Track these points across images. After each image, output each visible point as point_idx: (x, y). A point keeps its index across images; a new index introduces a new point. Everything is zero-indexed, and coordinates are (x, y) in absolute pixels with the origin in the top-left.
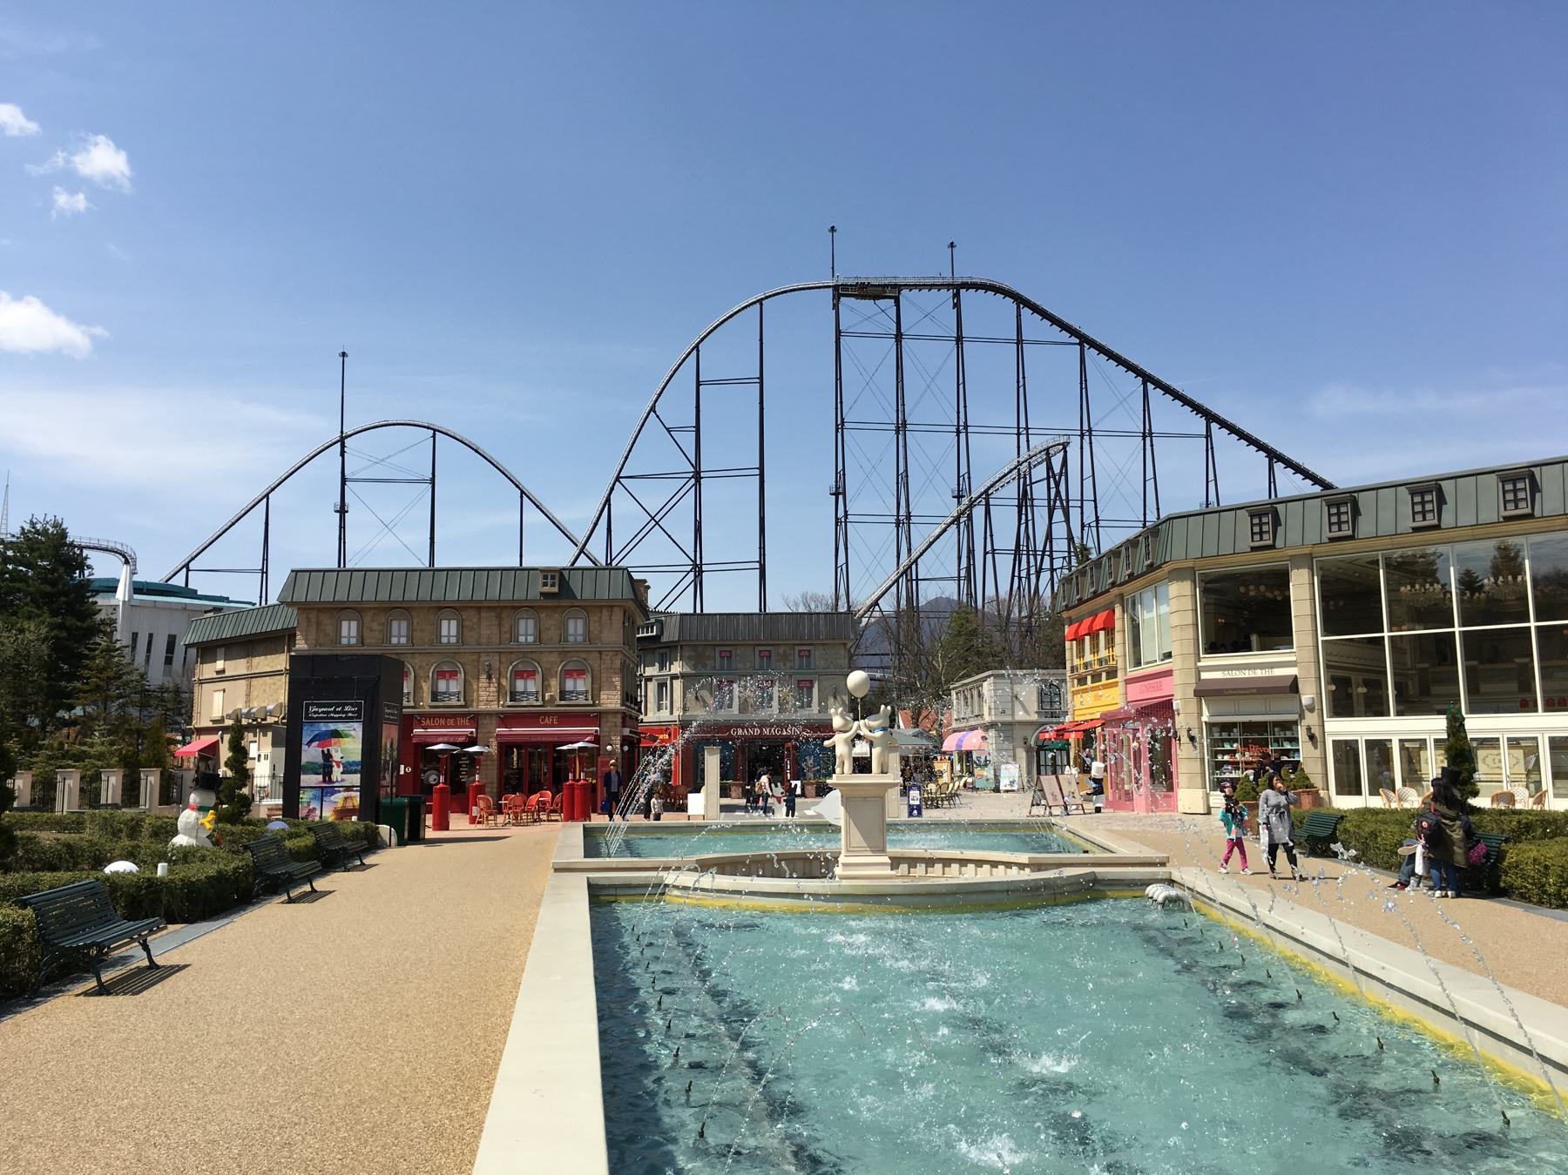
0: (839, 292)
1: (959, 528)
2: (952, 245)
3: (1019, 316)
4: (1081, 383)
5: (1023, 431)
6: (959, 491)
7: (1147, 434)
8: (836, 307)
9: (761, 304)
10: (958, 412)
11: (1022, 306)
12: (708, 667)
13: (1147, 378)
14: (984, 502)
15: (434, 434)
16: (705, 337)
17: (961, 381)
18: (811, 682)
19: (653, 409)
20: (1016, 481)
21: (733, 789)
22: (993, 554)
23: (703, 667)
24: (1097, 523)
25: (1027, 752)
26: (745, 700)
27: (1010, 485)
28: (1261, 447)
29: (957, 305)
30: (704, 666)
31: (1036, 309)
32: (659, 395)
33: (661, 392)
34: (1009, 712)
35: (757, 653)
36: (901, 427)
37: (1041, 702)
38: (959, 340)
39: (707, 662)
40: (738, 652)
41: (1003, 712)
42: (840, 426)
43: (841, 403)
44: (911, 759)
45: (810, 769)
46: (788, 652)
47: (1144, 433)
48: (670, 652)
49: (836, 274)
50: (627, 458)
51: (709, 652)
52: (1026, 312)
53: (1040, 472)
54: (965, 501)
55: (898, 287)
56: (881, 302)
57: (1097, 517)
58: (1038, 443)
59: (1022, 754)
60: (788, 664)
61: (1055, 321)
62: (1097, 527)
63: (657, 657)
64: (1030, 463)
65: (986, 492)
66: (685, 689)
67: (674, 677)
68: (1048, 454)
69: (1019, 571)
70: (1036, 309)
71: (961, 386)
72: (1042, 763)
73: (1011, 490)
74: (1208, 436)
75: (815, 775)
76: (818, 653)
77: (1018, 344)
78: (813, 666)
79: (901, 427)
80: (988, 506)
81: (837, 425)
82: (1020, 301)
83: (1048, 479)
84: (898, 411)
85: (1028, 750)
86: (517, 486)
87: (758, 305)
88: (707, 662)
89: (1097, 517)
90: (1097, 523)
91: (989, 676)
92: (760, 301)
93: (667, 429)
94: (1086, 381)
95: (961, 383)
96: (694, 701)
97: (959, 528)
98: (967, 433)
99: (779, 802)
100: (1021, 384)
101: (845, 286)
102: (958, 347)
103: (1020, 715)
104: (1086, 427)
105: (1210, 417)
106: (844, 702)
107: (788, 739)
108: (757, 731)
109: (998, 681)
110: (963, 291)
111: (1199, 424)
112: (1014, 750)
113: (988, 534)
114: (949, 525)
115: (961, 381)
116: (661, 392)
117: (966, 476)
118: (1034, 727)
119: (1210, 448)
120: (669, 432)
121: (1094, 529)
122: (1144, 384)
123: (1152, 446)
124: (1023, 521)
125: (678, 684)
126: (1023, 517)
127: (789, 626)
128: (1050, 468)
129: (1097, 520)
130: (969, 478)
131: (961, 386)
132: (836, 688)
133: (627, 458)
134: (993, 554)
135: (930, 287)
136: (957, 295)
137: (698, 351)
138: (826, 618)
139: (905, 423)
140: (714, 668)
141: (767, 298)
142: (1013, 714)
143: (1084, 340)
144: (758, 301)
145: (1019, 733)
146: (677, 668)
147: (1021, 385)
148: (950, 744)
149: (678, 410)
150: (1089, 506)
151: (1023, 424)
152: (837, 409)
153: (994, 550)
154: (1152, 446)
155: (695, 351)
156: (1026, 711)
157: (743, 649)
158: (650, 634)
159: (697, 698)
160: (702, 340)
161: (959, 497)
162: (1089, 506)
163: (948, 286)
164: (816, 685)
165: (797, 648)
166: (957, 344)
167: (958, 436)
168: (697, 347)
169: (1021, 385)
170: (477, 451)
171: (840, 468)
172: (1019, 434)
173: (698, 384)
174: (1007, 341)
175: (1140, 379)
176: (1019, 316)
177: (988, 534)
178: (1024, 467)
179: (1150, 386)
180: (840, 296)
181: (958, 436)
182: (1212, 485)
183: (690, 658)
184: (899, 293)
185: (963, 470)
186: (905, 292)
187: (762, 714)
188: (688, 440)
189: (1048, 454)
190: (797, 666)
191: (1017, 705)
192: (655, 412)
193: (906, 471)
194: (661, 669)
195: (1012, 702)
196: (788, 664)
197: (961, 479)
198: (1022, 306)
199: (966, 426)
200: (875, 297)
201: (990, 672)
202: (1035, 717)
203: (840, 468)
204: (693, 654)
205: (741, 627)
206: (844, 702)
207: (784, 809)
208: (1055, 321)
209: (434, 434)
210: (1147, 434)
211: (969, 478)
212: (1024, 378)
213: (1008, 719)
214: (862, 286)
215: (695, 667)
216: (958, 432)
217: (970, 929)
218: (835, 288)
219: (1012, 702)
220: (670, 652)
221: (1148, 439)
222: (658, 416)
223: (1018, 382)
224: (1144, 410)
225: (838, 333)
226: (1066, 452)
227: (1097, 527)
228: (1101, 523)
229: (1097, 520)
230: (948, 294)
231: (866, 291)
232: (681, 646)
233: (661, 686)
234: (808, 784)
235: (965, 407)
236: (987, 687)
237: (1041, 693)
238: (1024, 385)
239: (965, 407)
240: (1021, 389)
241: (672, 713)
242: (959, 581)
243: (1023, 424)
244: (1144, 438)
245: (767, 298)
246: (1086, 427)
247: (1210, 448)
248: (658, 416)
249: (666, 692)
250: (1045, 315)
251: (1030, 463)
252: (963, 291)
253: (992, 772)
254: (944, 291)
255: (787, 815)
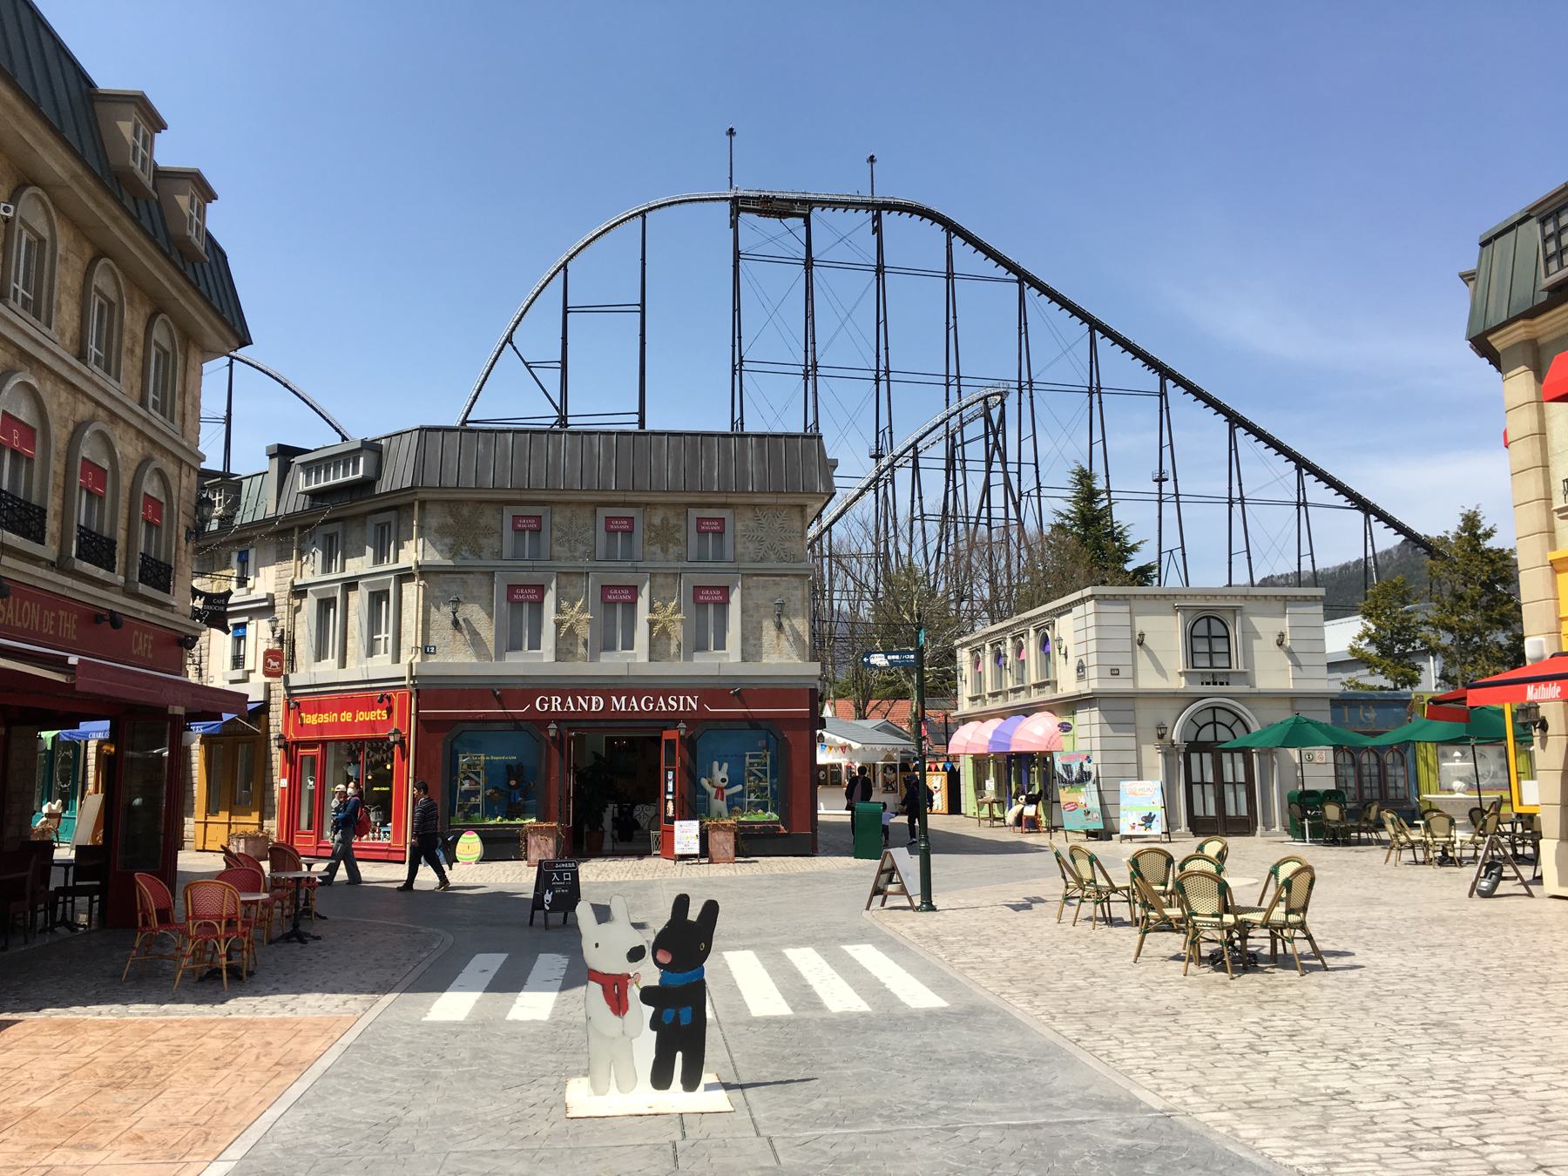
0: (739, 205)
1: (877, 493)
2: (872, 159)
3: (949, 245)
4: (1020, 328)
5: (953, 381)
6: (877, 450)
7: (1094, 390)
8: (734, 224)
9: (644, 217)
10: (878, 356)
11: (952, 234)
12: (486, 553)
13: (1095, 325)
14: (910, 464)
15: (231, 363)
16: (575, 254)
17: (881, 318)
18: (726, 591)
19: (509, 340)
20: (944, 441)
21: (532, 841)
22: (923, 520)
23: (473, 552)
24: (1039, 491)
25: (1165, 755)
26: (571, 630)
27: (935, 446)
28: (1220, 408)
29: (878, 230)
30: (477, 552)
31: (969, 238)
32: (518, 322)
33: (520, 320)
34: (1125, 672)
35: (601, 523)
36: (811, 370)
37: (1191, 654)
38: (880, 270)
39: (484, 542)
40: (557, 519)
41: (1115, 672)
42: (737, 367)
43: (740, 337)
44: (879, 769)
45: (720, 790)
46: (673, 521)
47: (1090, 388)
48: (398, 520)
49: (735, 185)
50: (475, 398)
51: (488, 518)
52: (957, 241)
53: (976, 428)
54: (885, 462)
55: (810, 203)
56: (790, 221)
57: (1038, 483)
58: (970, 395)
59: (1154, 759)
60: (673, 549)
61: (990, 253)
62: (1039, 497)
63: (370, 530)
64: (961, 415)
65: (914, 445)
66: (429, 602)
67: (404, 576)
68: (986, 403)
69: (947, 546)
70: (969, 238)
71: (882, 326)
72: (1196, 777)
73: (940, 450)
74: (1163, 394)
75: (730, 807)
76: (739, 526)
77: (948, 278)
78: (729, 554)
79: (811, 370)
80: (916, 468)
81: (734, 366)
82: (951, 228)
83: (986, 435)
84: (806, 351)
85: (1169, 751)
86: (338, 431)
87: (640, 218)
88: (484, 542)
89: (1038, 483)
90: (1039, 491)
91: (1082, 601)
92: (643, 214)
93: (526, 364)
94: (1026, 324)
95: (881, 321)
96: (448, 631)
97: (877, 493)
98: (888, 381)
99: (618, 1004)
100: (951, 324)
101: (746, 199)
102: (878, 279)
103: (1149, 681)
104: (1025, 378)
105: (1165, 373)
106: (798, 638)
107: (672, 720)
108: (597, 703)
109: (1105, 608)
110: (884, 213)
111: (1152, 380)
112: (1138, 750)
113: (916, 495)
114: (862, 493)
115: (881, 318)
116: (520, 320)
117: (887, 431)
118: (1179, 704)
119: (1164, 408)
120: (529, 368)
121: (1035, 500)
122: (1091, 330)
123: (1100, 402)
124: (951, 488)
125: (412, 593)
126: (951, 483)
127: (677, 463)
128: (988, 420)
129: (1039, 487)
130: (891, 433)
131: (882, 326)
132: (782, 605)
133: (475, 398)
134: (923, 520)
135: (847, 205)
136: (877, 218)
137: (566, 271)
138: (760, 446)
139: (815, 366)
140: (499, 555)
141: (651, 209)
142: (1134, 677)
143: (1025, 278)
144: (640, 213)
145: (1147, 716)
146: (411, 554)
147: (951, 325)
148: (970, 739)
149: (540, 340)
150: (1028, 471)
151: (953, 372)
152: (734, 346)
153: (923, 515)
154: (1100, 402)
155: (562, 271)
156: (1161, 671)
157: (568, 513)
158: (351, 477)
159: (456, 623)
160: (571, 257)
161: (877, 457)
162: (1028, 471)
163: (868, 206)
164: (735, 598)
165: (694, 513)
166: (878, 275)
167: (877, 384)
168: (565, 265)
169: (951, 325)
170: (286, 386)
171: (737, 416)
172: (948, 385)
173: (566, 312)
174: (932, 274)
175: (1086, 326)
176: (949, 245)
177: (916, 495)
178: (954, 421)
179: (1098, 334)
180: (739, 210)
181: (877, 384)
182: (1167, 451)
183: (442, 531)
184: (810, 210)
185: (884, 424)
186: (817, 210)
187: (612, 664)
188: (552, 379)
189: (986, 403)
190: (692, 555)
191: (1143, 659)
192: (511, 343)
193: (816, 421)
194: (378, 559)
195: (1133, 651)
196: (673, 549)
197: (881, 435)
198: (952, 234)
199: (887, 372)
200: (782, 215)
201: (1088, 591)
202: (1180, 684)
203: (737, 416)
204: (450, 521)
205: (564, 460)
206: (798, 638)
207: (645, 1044)
208: (990, 253)
209: (231, 363)
210: (1094, 390)
211: (891, 433)
212: (955, 317)
213: (1121, 685)
214: (767, 200)
215: (454, 551)
216: (877, 380)
217: (189, 363)
218: (734, 201)
219: (1133, 651)
220: (398, 520)
221: (1096, 396)
222: (515, 348)
223: (948, 323)
224: (1091, 362)
225: (737, 255)
226: (1003, 406)
227: (1039, 497)
228: (1044, 492)
229: (1039, 487)
230: (865, 217)
231: (772, 207)
232: (423, 503)
233: (378, 598)
234: (717, 828)
235: (887, 348)
236: (1066, 628)
237: (1191, 637)
238: (955, 326)
239: (887, 348)
240: (952, 332)
241: (397, 659)
242: (923, 515)
243: (953, 372)
244: (1091, 393)
245: (651, 209)
246: (1025, 378)
247: (1164, 408)
248: (515, 348)
249: (387, 611)
250: (980, 246)
251: (961, 415)
252: (884, 213)
253: (1095, 795)
254: (862, 212)
255: (661, 1078)
